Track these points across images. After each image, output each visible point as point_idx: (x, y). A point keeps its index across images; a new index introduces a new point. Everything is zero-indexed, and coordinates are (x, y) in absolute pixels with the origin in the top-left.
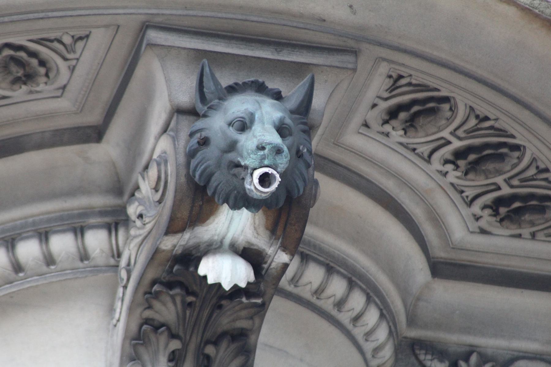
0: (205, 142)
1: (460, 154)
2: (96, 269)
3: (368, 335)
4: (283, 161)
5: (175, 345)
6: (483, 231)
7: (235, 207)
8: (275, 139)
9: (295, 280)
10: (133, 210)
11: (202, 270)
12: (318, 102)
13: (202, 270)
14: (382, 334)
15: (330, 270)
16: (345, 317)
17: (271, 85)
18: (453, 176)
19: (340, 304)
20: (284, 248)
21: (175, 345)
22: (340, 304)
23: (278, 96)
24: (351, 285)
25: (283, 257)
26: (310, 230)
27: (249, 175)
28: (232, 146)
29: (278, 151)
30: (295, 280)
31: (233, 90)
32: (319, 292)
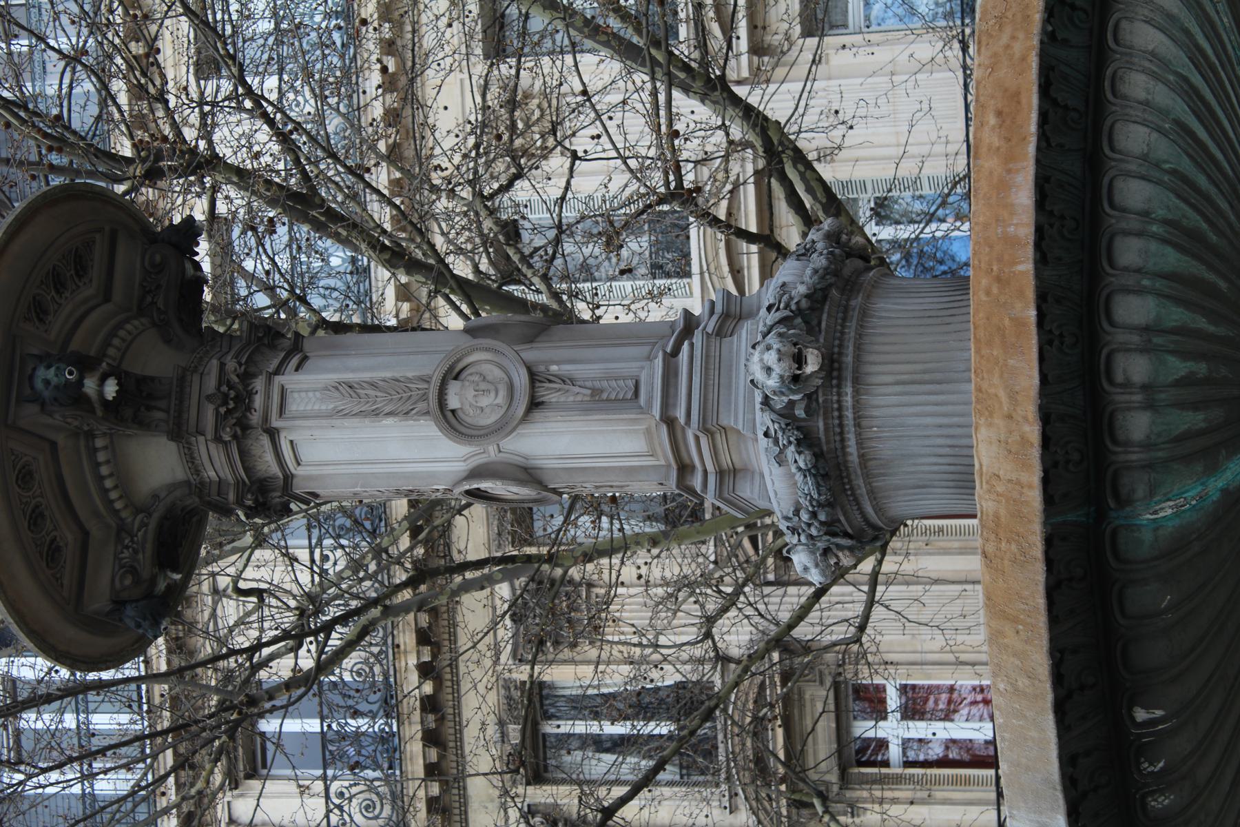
0: (55, 399)
1: (58, 292)
2: (112, 442)
3: (130, 333)
4: (62, 366)
5: (143, 409)
6: (91, 281)
7: (82, 385)
8: (52, 370)
9: (114, 359)
10: (86, 428)
11: (111, 399)
12: (36, 352)
13: (111, 399)
14: (136, 323)
15: (110, 345)
16: (129, 338)
17: (29, 371)
18: (67, 294)
19: (123, 340)
20: (100, 364)
21: (143, 409)
22: (123, 340)
23: (34, 369)
24: (116, 336)
25: (104, 364)
26: (92, 353)
27: (98, 374)
28: (57, 387)
29: (58, 368)
30: (114, 359)
31: (32, 387)
32: (119, 350)
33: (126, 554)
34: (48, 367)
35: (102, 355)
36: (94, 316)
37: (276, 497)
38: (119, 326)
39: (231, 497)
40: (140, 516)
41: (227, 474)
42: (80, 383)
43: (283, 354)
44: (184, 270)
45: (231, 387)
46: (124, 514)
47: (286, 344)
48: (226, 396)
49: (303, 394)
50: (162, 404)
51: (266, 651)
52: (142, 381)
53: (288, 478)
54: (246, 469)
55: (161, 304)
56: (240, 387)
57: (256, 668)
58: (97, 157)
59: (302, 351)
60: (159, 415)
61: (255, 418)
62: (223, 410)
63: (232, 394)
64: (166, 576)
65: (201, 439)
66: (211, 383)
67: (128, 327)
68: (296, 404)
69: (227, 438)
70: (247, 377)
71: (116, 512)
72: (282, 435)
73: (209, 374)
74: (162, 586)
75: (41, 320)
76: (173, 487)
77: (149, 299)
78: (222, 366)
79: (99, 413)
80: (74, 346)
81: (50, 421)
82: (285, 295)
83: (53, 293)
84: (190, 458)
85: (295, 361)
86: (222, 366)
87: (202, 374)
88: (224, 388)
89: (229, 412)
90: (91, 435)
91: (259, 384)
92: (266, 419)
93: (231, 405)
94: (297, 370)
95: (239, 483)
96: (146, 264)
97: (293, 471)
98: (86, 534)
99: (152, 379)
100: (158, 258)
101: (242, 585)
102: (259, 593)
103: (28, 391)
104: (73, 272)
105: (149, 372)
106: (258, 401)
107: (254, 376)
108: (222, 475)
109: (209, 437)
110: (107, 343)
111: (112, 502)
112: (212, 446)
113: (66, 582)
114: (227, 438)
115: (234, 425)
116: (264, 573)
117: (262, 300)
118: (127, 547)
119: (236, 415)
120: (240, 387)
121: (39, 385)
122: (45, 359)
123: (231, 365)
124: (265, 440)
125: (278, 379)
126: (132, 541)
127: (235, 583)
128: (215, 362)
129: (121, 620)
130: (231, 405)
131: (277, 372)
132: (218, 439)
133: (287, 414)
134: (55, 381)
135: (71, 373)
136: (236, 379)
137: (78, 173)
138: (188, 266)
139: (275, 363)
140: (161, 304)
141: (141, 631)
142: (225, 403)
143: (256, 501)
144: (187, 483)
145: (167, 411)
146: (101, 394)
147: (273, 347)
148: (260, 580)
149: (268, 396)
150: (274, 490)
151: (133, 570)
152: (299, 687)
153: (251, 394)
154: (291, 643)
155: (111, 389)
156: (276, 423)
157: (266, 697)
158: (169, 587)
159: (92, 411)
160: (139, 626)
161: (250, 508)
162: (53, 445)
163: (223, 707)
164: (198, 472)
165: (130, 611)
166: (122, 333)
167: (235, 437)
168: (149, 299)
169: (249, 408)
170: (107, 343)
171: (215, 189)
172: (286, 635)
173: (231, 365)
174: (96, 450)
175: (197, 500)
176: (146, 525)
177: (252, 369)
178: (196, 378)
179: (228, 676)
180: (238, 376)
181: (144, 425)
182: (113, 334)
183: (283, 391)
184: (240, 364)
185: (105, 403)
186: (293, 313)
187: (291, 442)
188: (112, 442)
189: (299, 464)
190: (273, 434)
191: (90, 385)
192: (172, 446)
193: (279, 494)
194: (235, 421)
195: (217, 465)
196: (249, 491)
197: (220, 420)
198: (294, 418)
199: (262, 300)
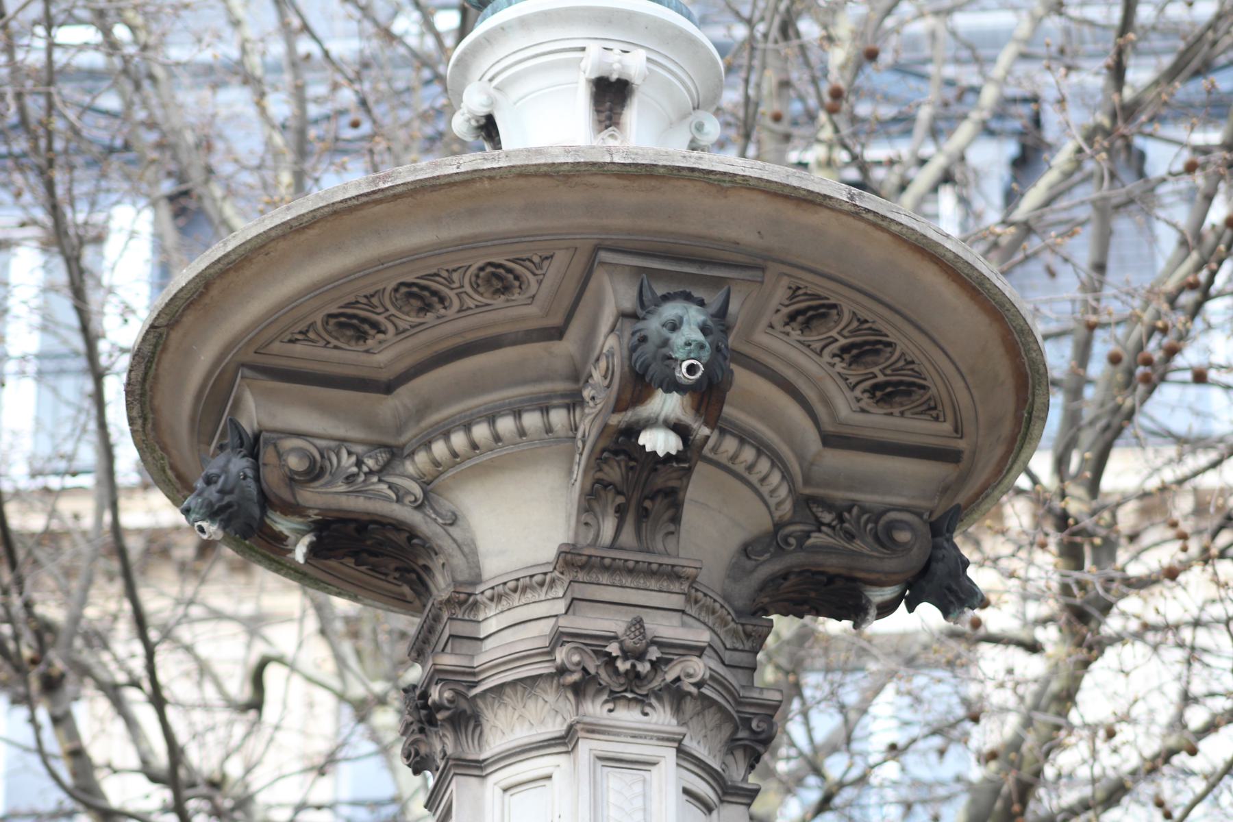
2: (558, 440)
4: (706, 355)
6: (863, 411)
8: (700, 337)
10: (587, 393)
12: (733, 307)
14: (783, 492)
23: (701, 303)
26: (727, 410)
28: (665, 343)
29: (702, 346)
31: (666, 298)
33: (348, 462)
34: (704, 329)
35: (723, 428)
36: (794, 412)
37: (442, 743)
38: (777, 460)
39: (448, 661)
40: (417, 490)
41: (489, 652)
42: (673, 386)
43: (716, 766)
44: (881, 584)
45: (655, 665)
46: (421, 458)
47: (736, 772)
48: (640, 656)
49: (639, 803)
50: (628, 537)
51: (145, 715)
52: (673, 500)
53: (477, 768)
54: (499, 689)
55: (816, 539)
56: (656, 683)
57: (113, 692)
58: (1107, 428)
59: (722, 801)
60: (608, 527)
61: (595, 709)
62: (614, 649)
63: (643, 668)
64: (303, 533)
65: (560, 606)
66: (666, 628)
67: (776, 478)
68: (616, 782)
69: (561, 655)
70: (675, 695)
71: (427, 445)
72: (562, 760)
73: (683, 625)
74: (283, 524)
75: (792, 317)
76: (470, 552)
77: (827, 517)
78: (699, 651)
79: (615, 420)
80: (743, 378)
81: (604, 327)
82: (835, 767)
83: (843, 342)
84: (521, 586)
85: (704, 789)
86: (699, 651)
87: (683, 612)
88: (654, 653)
89: (610, 660)
90: (574, 402)
91: (662, 718)
92: (594, 730)
93: (623, 666)
94: (686, 791)
95: (470, 676)
96: (893, 515)
97: (491, 780)
98: (388, 388)
99: (676, 519)
100: (903, 536)
101: (273, 675)
102: (256, 704)
103: (660, 291)
104: (881, 378)
105: (689, 514)
106: (628, 716)
107: (677, 710)
108: (488, 644)
109: (562, 622)
110: (744, 438)
111: (446, 436)
112: (546, 627)
113: (299, 348)
114: (561, 655)
115: (584, 670)
116: (295, 718)
117: (826, 723)
118: (359, 463)
119: (603, 675)
120: (656, 683)
121: (671, 311)
122: (718, 325)
123: (698, 667)
124: (556, 727)
125: (669, 755)
126: (371, 472)
127: (280, 660)
128: (703, 636)
129: (221, 447)
130: (623, 666)
131: (683, 753)
132: (559, 638)
133: (599, 763)
134: (678, 339)
135: (691, 369)
136: (670, 677)
137: (1075, 393)
138: (888, 593)
139: (700, 750)
140: (816, 539)
141: (200, 484)
142: (626, 654)
143: (439, 707)
144: (477, 580)
145: (613, 546)
146: (650, 423)
147: (732, 745)
148: (285, 705)
149: (637, 735)
150: (457, 741)
151: (315, 472)
152: (75, 774)
153: (641, 701)
154: (161, 759)
155: (659, 441)
156: (587, 747)
157: (59, 711)
158: (279, 538)
159: (619, 407)
160: (209, 481)
161: (425, 695)
162: (558, 333)
163: (44, 631)
164: (497, 598)
165: (239, 464)
166: (764, 465)
167: (562, 671)
168: (827, 517)
169: (614, 697)
170: (744, 438)
171: (1033, 647)
172: (175, 752)
173: (698, 667)
174: (545, 410)
175: (445, 596)
176: (399, 500)
177: (689, 706)
178: (676, 601)
179: (99, 639)
180: (678, 679)
181: (591, 499)
182: (763, 448)
183: (647, 764)
184: (699, 685)
185: (632, 431)
186: (791, 786)
187: (549, 777)
188: (558, 440)
189: (505, 790)
190: (566, 741)
191: (667, 404)
192: (548, 553)
193: (450, 751)
194: (592, 671)
195: (508, 636)
196: (457, 693)
197: (595, 644)
198: (594, 784)
199: (826, 723)
